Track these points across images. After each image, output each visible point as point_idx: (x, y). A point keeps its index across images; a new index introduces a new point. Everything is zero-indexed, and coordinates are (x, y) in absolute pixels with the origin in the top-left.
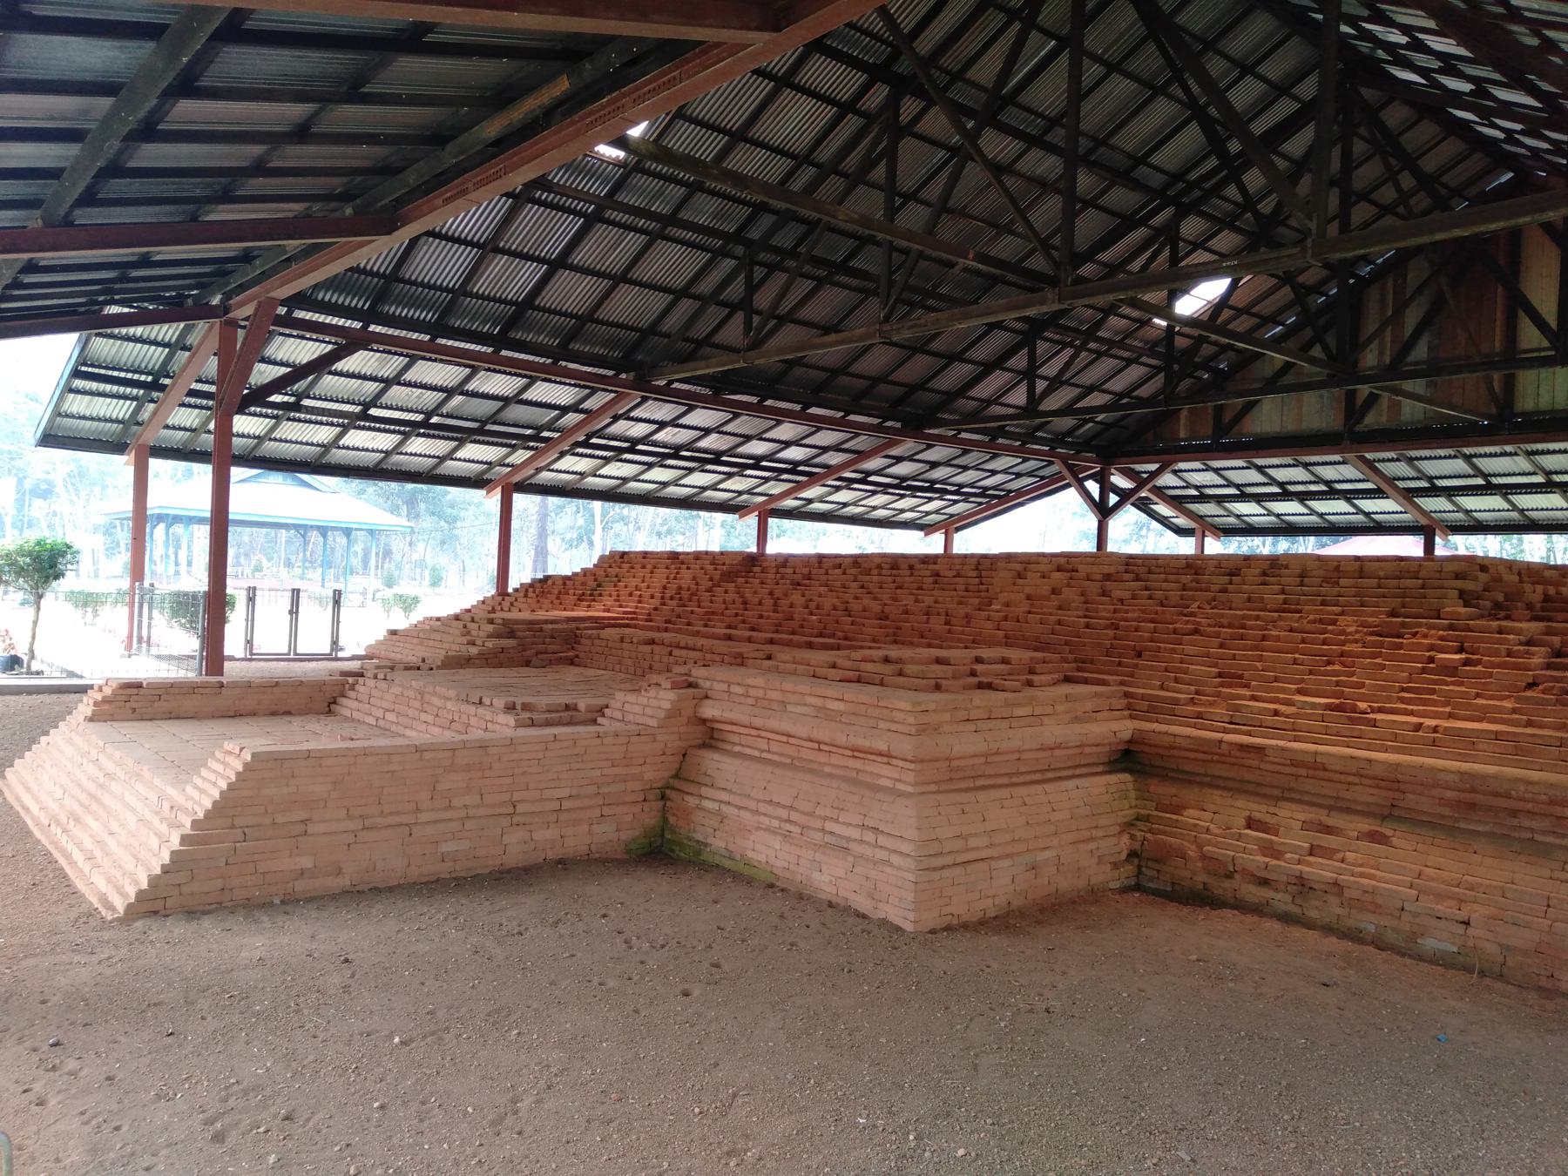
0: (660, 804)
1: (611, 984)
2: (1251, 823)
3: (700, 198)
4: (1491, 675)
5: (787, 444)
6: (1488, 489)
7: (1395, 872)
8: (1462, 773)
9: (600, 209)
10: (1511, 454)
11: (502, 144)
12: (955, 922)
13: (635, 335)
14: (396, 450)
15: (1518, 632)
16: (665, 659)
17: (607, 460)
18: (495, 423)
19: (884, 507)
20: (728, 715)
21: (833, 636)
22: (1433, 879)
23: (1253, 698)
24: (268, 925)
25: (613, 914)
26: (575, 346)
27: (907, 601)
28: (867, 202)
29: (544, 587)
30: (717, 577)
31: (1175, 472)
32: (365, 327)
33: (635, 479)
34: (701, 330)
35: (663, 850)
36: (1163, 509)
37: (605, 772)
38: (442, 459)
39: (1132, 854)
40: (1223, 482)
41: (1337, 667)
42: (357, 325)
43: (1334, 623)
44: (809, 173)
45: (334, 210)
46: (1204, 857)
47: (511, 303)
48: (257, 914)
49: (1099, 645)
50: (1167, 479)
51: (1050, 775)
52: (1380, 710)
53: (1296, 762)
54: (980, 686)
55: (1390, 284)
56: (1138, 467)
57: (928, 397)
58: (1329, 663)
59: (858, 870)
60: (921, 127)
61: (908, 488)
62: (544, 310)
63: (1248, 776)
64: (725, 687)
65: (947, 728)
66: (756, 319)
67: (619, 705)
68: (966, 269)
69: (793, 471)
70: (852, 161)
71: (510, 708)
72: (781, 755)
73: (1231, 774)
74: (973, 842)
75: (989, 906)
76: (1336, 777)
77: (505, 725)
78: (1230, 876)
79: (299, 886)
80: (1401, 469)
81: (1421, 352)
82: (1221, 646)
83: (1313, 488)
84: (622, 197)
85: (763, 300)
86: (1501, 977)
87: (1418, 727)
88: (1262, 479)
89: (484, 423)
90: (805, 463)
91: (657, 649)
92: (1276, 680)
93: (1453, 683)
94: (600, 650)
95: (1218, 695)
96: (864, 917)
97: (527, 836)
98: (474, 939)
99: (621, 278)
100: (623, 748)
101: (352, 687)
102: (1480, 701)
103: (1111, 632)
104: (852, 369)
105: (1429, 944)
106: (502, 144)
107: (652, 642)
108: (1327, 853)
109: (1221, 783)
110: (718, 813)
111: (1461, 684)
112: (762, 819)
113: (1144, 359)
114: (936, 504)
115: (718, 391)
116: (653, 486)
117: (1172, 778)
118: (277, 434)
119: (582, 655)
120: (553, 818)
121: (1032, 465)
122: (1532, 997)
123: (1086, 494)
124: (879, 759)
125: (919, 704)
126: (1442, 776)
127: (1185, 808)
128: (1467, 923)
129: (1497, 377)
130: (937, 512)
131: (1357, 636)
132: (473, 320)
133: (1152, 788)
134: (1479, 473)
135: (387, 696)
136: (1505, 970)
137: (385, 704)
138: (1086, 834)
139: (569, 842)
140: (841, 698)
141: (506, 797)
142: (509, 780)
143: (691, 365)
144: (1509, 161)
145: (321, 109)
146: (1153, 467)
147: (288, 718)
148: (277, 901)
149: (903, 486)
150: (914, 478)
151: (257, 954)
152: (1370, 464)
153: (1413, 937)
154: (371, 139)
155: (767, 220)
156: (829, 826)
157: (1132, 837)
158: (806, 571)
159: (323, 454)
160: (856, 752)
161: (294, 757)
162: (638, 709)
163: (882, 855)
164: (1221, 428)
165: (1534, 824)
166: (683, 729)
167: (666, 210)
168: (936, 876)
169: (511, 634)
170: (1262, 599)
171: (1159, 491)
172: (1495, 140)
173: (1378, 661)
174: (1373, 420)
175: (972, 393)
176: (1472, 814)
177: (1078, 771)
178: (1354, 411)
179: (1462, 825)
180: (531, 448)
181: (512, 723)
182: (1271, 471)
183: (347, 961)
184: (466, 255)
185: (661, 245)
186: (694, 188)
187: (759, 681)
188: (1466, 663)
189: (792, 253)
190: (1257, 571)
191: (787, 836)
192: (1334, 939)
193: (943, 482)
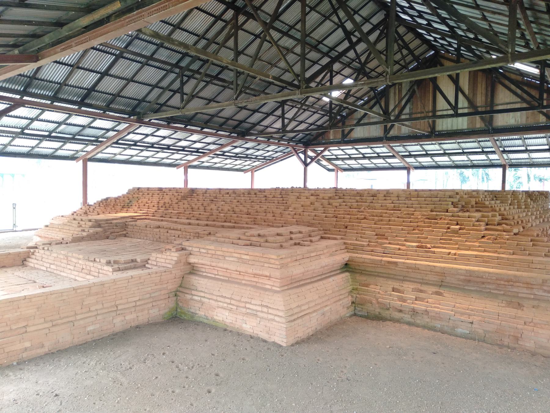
0: (175, 298)
1: (177, 391)
2: (394, 290)
3: (162, 50)
4: (470, 233)
5: (195, 142)
6: (427, 155)
7: (447, 306)
8: (466, 270)
9: (122, 53)
10: (434, 144)
11: (87, 28)
12: (299, 339)
14: (37, 146)
15: (474, 217)
16: (166, 234)
17: (125, 149)
18: (79, 135)
19: (239, 164)
20: (200, 261)
21: (230, 222)
22: (459, 308)
23: (390, 243)
24: (13, 377)
25: (167, 353)
26: (112, 106)
27: (257, 207)
28: (226, 56)
29: (107, 204)
30: (180, 198)
31: (329, 150)
32: (21, 98)
33: (136, 155)
34: (162, 100)
35: (178, 318)
36: (324, 163)
37: (153, 288)
38: (57, 150)
39: (353, 303)
40: (344, 153)
41: (417, 231)
42: (18, 97)
43: (413, 214)
44: (203, 42)
45: (10, 51)
46: (378, 303)
47: (85, 89)
48: (7, 372)
49: (331, 224)
50: (326, 153)
51: (323, 276)
52: (434, 247)
53: (409, 267)
54: (295, 244)
56: (316, 149)
57: (246, 125)
58: (414, 230)
59: (261, 323)
60: (245, 27)
61: (239, 157)
62: (99, 92)
63: (390, 272)
64: (198, 250)
65: (290, 265)
66: (185, 97)
67: (154, 259)
68: (260, 79)
69: (197, 152)
70: (220, 39)
71: (108, 263)
72: (224, 276)
73: (384, 271)
74: (303, 308)
75: (310, 331)
76: (423, 272)
77: (107, 274)
78: (388, 309)
79: (25, 355)
81: (407, 110)
82: (375, 224)
84: (130, 48)
85: (188, 89)
86: (484, 341)
87: (449, 253)
88: (357, 152)
89: (75, 135)
90: (202, 149)
91: (162, 230)
92: (396, 236)
93: (457, 237)
94: (137, 231)
95: (377, 242)
96: (265, 341)
97: (123, 318)
98: (112, 375)
99: (131, 80)
100: (159, 278)
101: (33, 254)
102: (467, 243)
103: (335, 219)
104: (219, 115)
105: (459, 330)
106: (87, 28)
107: (159, 227)
108: (422, 300)
109: (381, 275)
110: (200, 301)
111: (460, 237)
112: (219, 303)
113: (319, 112)
114: (248, 162)
115: (169, 122)
116: (143, 158)
117: (364, 274)
119: (129, 233)
120: (133, 310)
121: (281, 148)
122: (496, 348)
123: (300, 158)
124: (265, 278)
125: (279, 256)
126: (460, 271)
127: (370, 285)
128: (472, 323)
129: (430, 121)
130: (248, 165)
131: (422, 220)
132: (69, 95)
133: (357, 278)
135: (50, 258)
136: (485, 339)
137: (50, 261)
138: (338, 298)
139: (140, 318)
140: (247, 253)
141: (113, 303)
142: (114, 296)
143: (158, 114)
144: (432, 47)
145: (6, 9)
146: (322, 149)
147: (5, 269)
148: (15, 363)
149: (237, 156)
150: (241, 154)
151: (12, 396)
152: (391, 147)
153: (454, 328)
154: (29, 23)
155: (187, 60)
156: (248, 306)
157: (352, 297)
158: (215, 195)
159: (4, 148)
160: (255, 275)
161: (18, 300)
162: (163, 261)
163: (271, 317)
164: (344, 135)
165: (490, 287)
166: (182, 268)
167: (149, 54)
168: (293, 324)
169: (99, 226)
170: (386, 206)
171: (323, 157)
172: (430, 40)
173: (430, 229)
174: (393, 133)
175: (262, 124)
176: (470, 284)
177: (332, 274)
178: (387, 130)
179: (466, 288)
180: (95, 145)
181: (111, 270)
182: (360, 150)
183: (56, 395)
184: (65, 70)
185: (146, 67)
186: (161, 46)
187: (212, 247)
188: (460, 229)
189: (198, 72)
190: (382, 195)
191: (230, 310)
192: (426, 330)
193: (251, 155)
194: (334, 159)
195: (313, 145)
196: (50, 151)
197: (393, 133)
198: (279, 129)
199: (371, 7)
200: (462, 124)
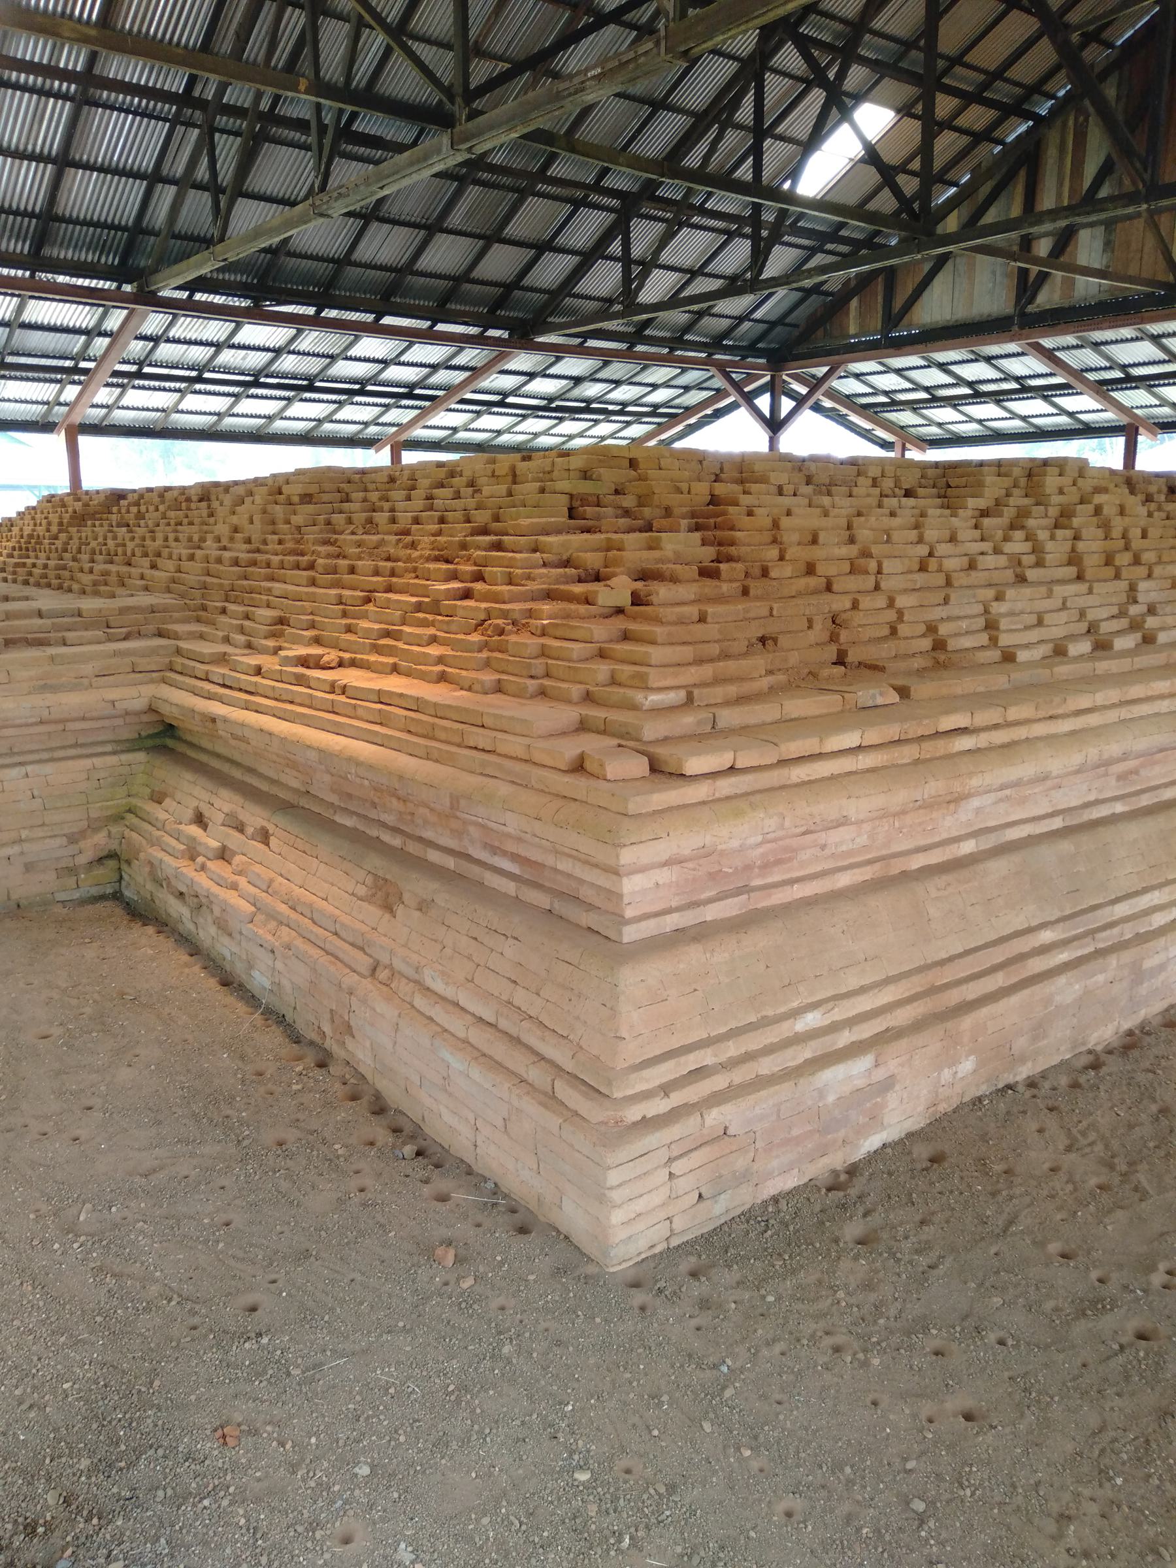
13: (443, 284)
26: (452, 306)
32: (190, 296)
33: (508, 430)
55: (1071, 123)
80: (1088, 357)
83: (1006, 386)
88: (949, 380)
90: (666, 404)
118: (125, 402)
164: (892, 319)
168: (775, 740)
174: (1047, 298)
178: (1026, 287)
194: (883, 404)
195: (797, 358)
196: (352, 429)
197: (1047, 298)
198: (609, 301)
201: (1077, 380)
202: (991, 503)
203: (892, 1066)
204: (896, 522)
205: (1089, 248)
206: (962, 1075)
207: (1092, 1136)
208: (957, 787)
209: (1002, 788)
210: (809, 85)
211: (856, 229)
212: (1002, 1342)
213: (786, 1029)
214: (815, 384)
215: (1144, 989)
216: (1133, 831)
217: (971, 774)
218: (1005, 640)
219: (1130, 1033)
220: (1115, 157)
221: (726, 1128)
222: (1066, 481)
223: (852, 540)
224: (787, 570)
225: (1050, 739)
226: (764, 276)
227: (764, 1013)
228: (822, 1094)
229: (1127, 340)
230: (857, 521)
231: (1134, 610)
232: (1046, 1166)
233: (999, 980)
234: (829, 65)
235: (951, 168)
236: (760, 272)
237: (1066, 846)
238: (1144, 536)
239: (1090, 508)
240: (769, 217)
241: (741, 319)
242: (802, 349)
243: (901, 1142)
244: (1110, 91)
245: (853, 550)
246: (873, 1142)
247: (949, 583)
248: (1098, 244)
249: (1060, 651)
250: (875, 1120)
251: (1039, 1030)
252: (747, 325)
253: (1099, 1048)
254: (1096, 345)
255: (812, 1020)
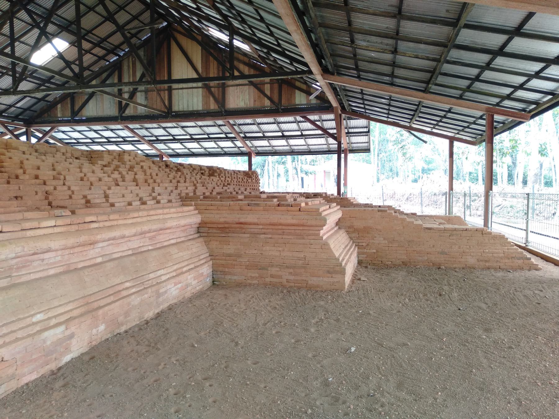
88: (312, 127)
134: (170, 135)
146: (48, 129)
164: (74, 113)
174: (129, 112)
178: (122, 108)
194: (74, 143)
195: (37, 123)
197: (129, 112)
199: (136, 7)
200: (198, 105)
201: (142, 139)
202: (107, 163)
203: (73, 329)
204: (72, 166)
205: (140, 98)
206: (101, 331)
207: (145, 340)
208: (93, 238)
209: (109, 240)
210: (33, 27)
211: (58, 79)
212: (112, 396)
213: (28, 321)
214: (45, 134)
215: (161, 299)
216: (155, 253)
217: (97, 234)
218: (111, 200)
219: (158, 313)
220: (145, 72)
221: (3, 358)
222: (131, 158)
223: (54, 170)
224: (27, 177)
225: (125, 225)
226: (18, 89)
227: (19, 317)
228: (44, 341)
229: (156, 128)
230: (56, 164)
231: (154, 194)
232: (130, 351)
233: (112, 299)
234: (41, 22)
235: (93, 65)
236: (17, 87)
237: (133, 258)
238: (157, 175)
239: (140, 166)
240: (19, 69)
241: (10, 106)
242: (39, 120)
243: (79, 357)
244: (141, 53)
245: (55, 173)
246: (67, 358)
247: (92, 184)
248: (143, 97)
249: (130, 204)
250: (68, 350)
251: (127, 314)
252: (13, 109)
253: (148, 319)
254: (146, 129)
255: (39, 317)
